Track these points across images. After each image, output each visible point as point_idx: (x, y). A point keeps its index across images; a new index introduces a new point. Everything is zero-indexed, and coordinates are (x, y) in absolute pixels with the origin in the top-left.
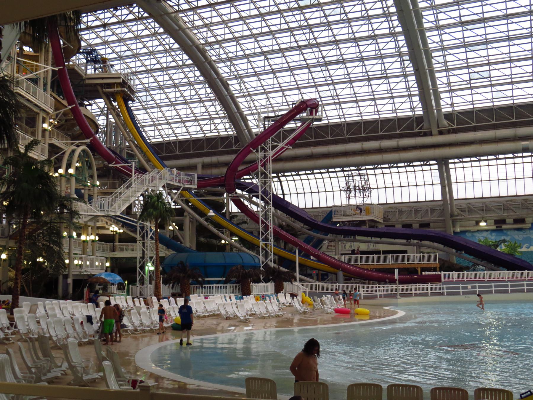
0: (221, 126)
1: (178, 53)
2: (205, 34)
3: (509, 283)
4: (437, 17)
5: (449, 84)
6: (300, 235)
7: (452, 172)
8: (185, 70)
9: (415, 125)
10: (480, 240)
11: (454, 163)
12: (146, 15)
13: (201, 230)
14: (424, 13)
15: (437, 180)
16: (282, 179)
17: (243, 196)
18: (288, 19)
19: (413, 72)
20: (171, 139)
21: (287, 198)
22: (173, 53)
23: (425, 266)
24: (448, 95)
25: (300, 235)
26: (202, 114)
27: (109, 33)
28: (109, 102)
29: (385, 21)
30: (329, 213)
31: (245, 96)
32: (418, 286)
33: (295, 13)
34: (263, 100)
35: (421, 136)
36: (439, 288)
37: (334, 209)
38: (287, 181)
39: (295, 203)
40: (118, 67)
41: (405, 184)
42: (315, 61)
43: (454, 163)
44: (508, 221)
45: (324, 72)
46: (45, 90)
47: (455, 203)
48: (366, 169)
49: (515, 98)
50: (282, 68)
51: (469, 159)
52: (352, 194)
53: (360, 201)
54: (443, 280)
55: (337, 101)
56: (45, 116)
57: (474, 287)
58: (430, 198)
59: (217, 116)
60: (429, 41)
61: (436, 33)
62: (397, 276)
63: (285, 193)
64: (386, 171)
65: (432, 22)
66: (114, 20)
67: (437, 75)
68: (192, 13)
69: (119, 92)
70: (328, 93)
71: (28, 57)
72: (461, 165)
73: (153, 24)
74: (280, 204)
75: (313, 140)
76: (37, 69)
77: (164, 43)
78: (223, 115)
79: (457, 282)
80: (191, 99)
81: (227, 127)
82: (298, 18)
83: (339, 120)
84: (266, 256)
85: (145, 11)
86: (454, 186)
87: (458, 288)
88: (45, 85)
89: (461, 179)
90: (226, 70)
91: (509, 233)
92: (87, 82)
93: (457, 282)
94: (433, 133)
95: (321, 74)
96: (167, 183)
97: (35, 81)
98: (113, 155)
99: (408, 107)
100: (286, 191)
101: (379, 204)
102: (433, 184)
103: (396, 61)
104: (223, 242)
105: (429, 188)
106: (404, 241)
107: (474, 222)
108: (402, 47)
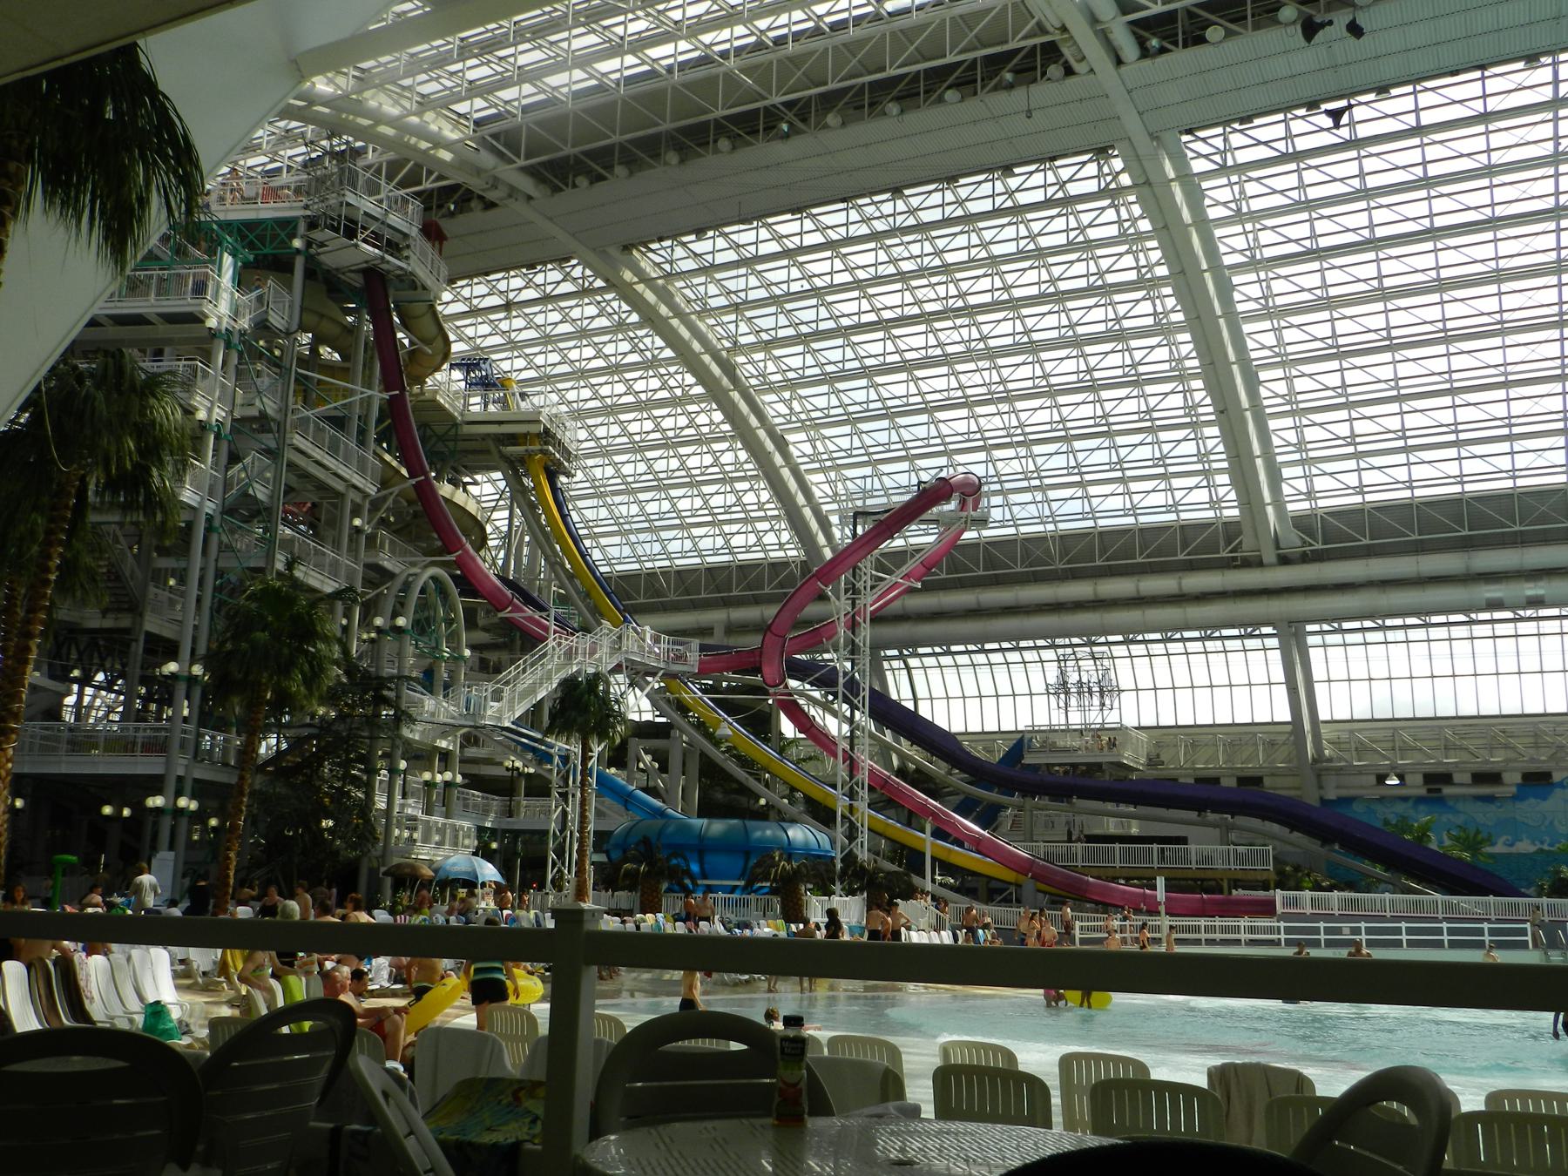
0: (770, 538)
1: (672, 369)
2: (732, 327)
3: (1445, 925)
4: (1269, 287)
5: (1301, 445)
6: (950, 794)
7: (1316, 655)
8: (691, 408)
9: (1222, 543)
10: (1387, 822)
11: (1321, 632)
12: (599, 283)
13: (710, 772)
14: (1236, 280)
15: (1278, 674)
16: (913, 662)
17: (802, 694)
18: (920, 294)
19: (1213, 417)
20: (658, 564)
21: (924, 711)
22: (663, 371)
23: (1240, 876)
24: (1298, 471)
25: (950, 794)
26: (727, 509)
27: (519, 323)
28: (514, 481)
29: (1144, 299)
30: (1020, 743)
31: (823, 470)
32: (1218, 922)
33: (934, 280)
34: (856, 469)
35: (1236, 567)
36: (1271, 930)
37: (1028, 736)
38: (924, 668)
39: (941, 722)
40: (544, 402)
41: (1194, 686)
42: (983, 390)
43: (1321, 632)
44: (1457, 778)
45: (1005, 417)
46: (362, 442)
47: (1324, 730)
48: (1107, 643)
49: (1460, 427)
50: (907, 405)
51: (1356, 625)
52: (1073, 701)
53: (1094, 717)
54: (1279, 909)
55: (1037, 483)
56: (358, 500)
57: (1356, 931)
58: (1262, 716)
59: (762, 514)
60: (1251, 344)
61: (1267, 325)
62: (1161, 894)
63: (919, 695)
64: (1158, 648)
65: (1225, 204)
66: (530, 294)
67: (1273, 424)
68: (702, 279)
69: (530, 455)
70: (1015, 466)
71: (329, 368)
72: (1337, 638)
73: (615, 304)
74: (888, 713)
75: (981, 573)
76: (352, 393)
77: (642, 346)
78: (776, 513)
79: (1315, 918)
80: (702, 474)
81: (783, 540)
82: (941, 290)
83: (1040, 528)
84: (852, 835)
85: (597, 275)
86: (1320, 690)
87: (1398, 931)
88: (362, 433)
89: (1338, 672)
90: (783, 409)
91: (1460, 806)
92: (467, 429)
93: (1315, 918)
94: (1265, 561)
95: (1015, 466)
96: (627, 660)
97: (339, 422)
98: (509, 593)
99: (1203, 500)
100: (922, 692)
101: (1139, 728)
102: (1270, 684)
103: (1172, 392)
104: (763, 802)
105: (1261, 693)
106: (1193, 815)
107: (1373, 780)
108: (1187, 358)
